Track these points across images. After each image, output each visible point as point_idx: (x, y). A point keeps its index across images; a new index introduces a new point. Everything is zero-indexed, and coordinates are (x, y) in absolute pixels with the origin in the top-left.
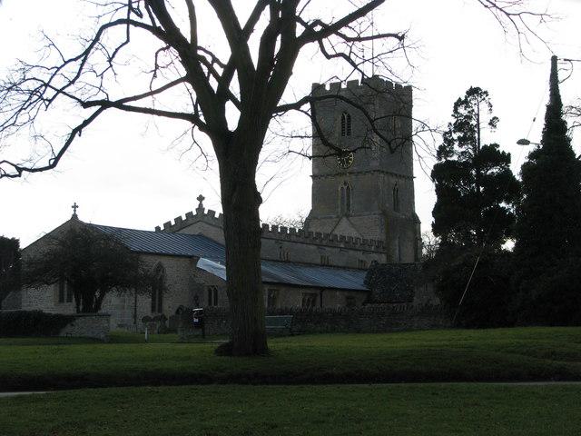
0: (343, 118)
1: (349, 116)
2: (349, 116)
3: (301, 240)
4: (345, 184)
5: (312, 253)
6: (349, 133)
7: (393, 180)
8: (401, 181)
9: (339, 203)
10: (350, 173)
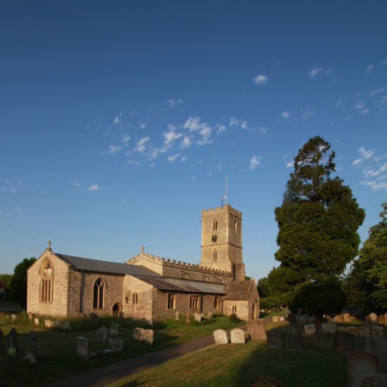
1: (217, 222)
2: (217, 222)
5: (200, 276)
6: (216, 229)
8: (237, 249)
9: (212, 257)
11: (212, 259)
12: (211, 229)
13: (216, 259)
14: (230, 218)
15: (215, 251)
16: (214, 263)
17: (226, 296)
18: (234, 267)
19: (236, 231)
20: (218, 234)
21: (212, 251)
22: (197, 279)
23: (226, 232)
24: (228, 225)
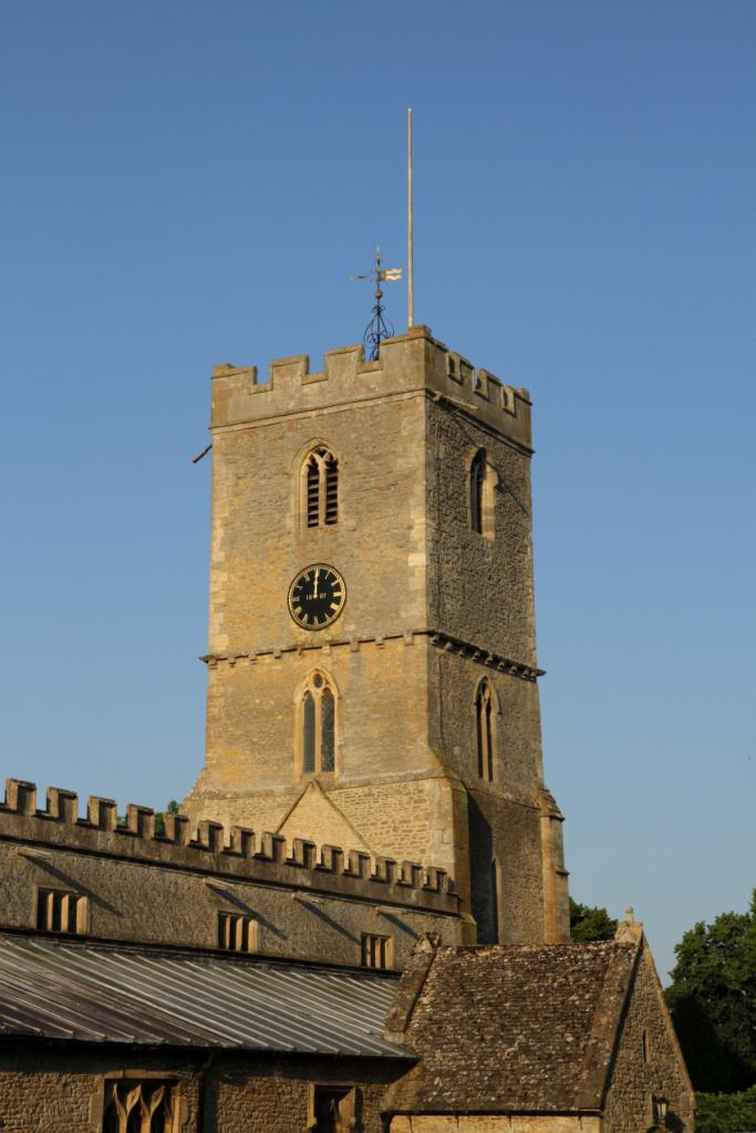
0: (313, 469)
1: (332, 466)
2: (332, 466)
3: (167, 857)
4: (318, 681)
6: (331, 517)
7: (478, 673)
8: (499, 680)
9: (297, 744)
10: (334, 644)
11: (298, 766)
12: (290, 523)
13: (329, 765)
14: (435, 432)
15: (317, 693)
16: (314, 797)
17: (411, 1082)
18: (478, 829)
19: (489, 535)
20: (340, 562)
21: (299, 698)
22: (168, 936)
23: (405, 545)
24: (419, 489)
